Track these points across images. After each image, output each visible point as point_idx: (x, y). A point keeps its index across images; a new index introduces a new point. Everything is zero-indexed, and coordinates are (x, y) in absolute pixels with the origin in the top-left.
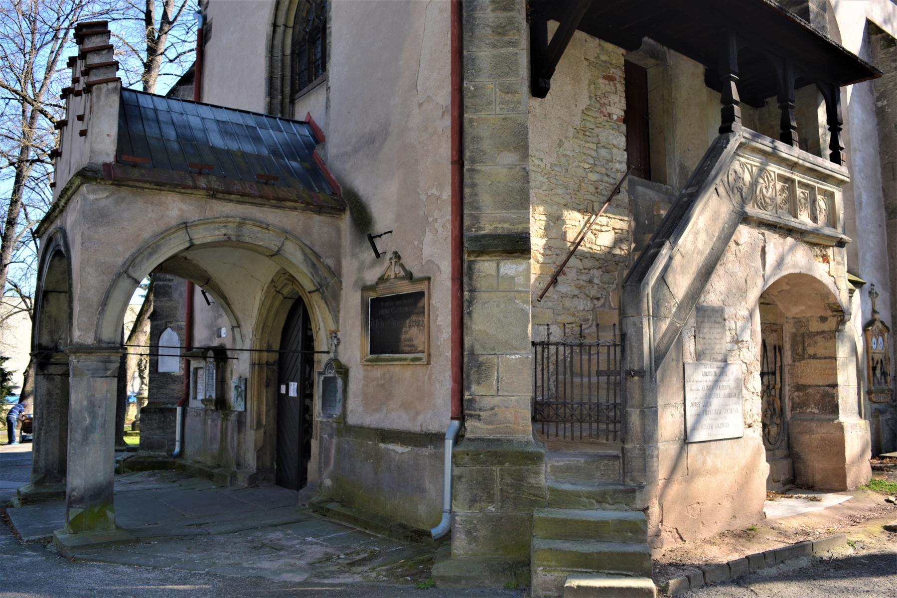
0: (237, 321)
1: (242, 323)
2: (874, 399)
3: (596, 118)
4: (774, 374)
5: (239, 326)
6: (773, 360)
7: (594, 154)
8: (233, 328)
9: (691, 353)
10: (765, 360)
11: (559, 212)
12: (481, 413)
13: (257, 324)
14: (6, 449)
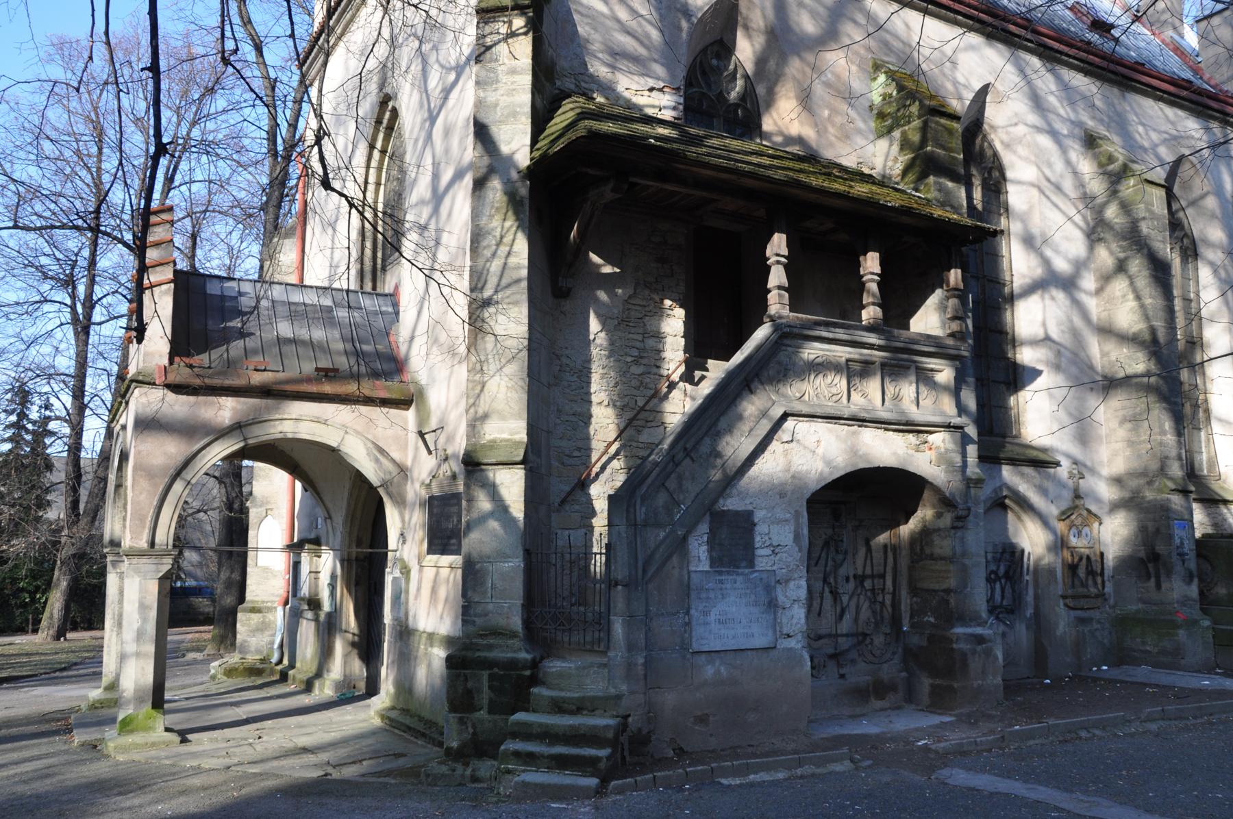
0: (328, 512)
1: (333, 515)
2: (1071, 605)
3: (645, 306)
4: (883, 576)
5: (330, 518)
6: (882, 561)
7: (638, 344)
8: (326, 518)
9: (51, 617)
10: (868, 562)
11: (945, 288)
12: (476, 619)
13: (347, 515)
14: (188, 720)
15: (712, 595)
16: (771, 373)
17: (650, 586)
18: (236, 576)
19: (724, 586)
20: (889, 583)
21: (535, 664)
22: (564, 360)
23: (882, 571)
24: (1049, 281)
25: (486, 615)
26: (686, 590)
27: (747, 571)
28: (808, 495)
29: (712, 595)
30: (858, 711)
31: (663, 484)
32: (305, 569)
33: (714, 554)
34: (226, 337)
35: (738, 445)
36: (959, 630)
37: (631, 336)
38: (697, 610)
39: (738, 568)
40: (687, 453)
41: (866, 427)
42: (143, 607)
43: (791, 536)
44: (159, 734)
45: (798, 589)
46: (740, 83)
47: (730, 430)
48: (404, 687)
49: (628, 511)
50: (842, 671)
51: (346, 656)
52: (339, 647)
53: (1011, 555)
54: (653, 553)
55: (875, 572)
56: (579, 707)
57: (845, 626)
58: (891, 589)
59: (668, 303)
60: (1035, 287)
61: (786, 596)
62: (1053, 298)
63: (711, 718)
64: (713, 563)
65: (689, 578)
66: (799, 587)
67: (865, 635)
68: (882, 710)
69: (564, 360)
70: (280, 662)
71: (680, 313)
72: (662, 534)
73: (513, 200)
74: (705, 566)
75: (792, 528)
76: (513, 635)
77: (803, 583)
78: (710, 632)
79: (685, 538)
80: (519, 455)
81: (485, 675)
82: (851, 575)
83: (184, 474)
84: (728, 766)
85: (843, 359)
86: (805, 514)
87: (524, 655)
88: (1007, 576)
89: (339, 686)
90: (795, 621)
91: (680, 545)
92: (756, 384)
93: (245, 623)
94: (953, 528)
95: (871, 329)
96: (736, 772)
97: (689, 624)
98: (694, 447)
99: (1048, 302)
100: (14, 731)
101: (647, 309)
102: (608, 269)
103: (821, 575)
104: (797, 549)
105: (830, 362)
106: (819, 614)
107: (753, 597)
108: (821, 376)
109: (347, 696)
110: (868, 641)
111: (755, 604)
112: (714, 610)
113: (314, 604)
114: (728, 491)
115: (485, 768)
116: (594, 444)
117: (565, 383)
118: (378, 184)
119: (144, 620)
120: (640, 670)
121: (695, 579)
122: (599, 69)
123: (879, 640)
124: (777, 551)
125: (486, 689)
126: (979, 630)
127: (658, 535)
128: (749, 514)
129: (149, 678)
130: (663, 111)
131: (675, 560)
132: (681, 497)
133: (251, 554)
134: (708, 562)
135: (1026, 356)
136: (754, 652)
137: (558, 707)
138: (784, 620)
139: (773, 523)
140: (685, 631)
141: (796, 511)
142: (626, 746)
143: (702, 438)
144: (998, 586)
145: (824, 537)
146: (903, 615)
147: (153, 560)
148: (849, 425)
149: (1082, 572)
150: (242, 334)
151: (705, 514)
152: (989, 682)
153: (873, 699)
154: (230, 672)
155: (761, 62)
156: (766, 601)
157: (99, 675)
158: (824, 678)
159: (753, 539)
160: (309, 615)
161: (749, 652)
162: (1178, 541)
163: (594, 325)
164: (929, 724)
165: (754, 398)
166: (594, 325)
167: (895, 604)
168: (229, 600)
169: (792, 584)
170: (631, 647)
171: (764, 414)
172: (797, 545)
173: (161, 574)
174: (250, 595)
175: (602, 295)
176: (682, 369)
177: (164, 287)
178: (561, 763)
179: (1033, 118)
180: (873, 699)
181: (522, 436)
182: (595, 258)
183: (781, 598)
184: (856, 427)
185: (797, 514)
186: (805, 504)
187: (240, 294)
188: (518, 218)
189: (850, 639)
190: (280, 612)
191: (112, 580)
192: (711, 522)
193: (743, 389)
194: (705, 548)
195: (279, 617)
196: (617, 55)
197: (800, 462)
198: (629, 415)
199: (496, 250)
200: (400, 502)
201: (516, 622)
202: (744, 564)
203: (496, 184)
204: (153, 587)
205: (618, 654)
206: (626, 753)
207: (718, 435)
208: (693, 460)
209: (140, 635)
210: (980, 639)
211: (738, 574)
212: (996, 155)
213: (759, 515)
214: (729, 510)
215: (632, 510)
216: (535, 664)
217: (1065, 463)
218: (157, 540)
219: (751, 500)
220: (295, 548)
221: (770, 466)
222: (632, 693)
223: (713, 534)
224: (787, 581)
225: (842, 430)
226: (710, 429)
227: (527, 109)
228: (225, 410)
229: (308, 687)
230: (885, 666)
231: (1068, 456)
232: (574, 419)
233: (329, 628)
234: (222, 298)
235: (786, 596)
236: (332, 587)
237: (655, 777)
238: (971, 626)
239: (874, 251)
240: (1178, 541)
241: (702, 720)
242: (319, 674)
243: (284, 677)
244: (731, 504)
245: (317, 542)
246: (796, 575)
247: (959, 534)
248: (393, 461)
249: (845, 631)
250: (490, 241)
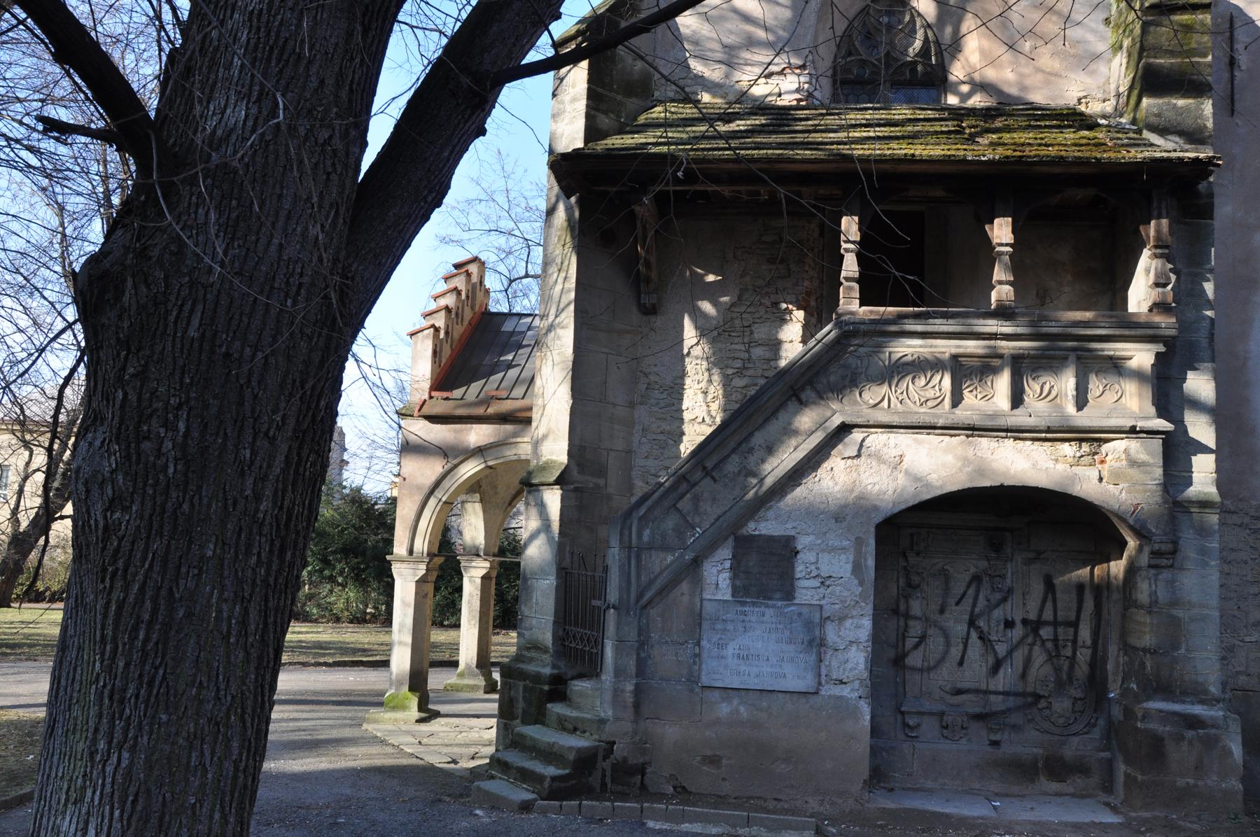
4: (1075, 625)
15: (730, 627)
16: (832, 378)
17: (653, 612)
19: (747, 619)
20: (1085, 634)
22: (652, 378)
23: (1073, 617)
25: (531, 629)
26: (697, 620)
27: (780, 603)
28: (879, 518)
29: (730, 627)
30: (1015, 789)
31: (674, 505)
33: (738, 583)
37: (733, 346)
38: (709, 641)
39: (770, 599)
40: (707, 473)
41: (982, 436)
43: (849, 567)
45: (861, 627)
46: (920, 34)
49: (622, 534)
50: (994, 737)
54: (656, 578)
55: (1059, 619)
57: (1006, 678)
58: (1089, 642)
61: (839, 636)
63: (724, 761)
64: (735, 591)
65: (701, 606)
66: (858, 627)
67: (1038, 697)
68: (1058, 794)
69: (652, 378)
72: (670, 558)
74: (725, 593)
75: (851, 558)
77: (867, 623)
78: (726, 667)
79: (696, 563)
81: (521, 684)
82: (1018, 620)
83: (436, 493)
84: (660, 809)
85: (947, 355)
86: (872, 542)
90: (849, 666)
92: (808, 394)
94: (1150, 566)
95: (1003, 313)
96: (667, 817)
97: (698, 655)
98: (716, 466)
100: (352, 698)
101: (756, 315)
102: (711, 278)
103: (967, 617)
104: (856, 582)
105: (927, 360)
106: (961, 663)
107: (787, 633)
108: (909, 378)
110: (1043, 704)
111: (790, 642)
112: (731, 643)
114: (761, 513)
117: (653, 401)
120: (629, 698)
121: (709, 608)
123: (1061, 705)
124: (828, 583)
125: (521, 699)
126: (1198, 710)
127: (665, 559)
130: (783, 97)
131: (685, 586)
132: (697, 520)
134: (730, 590)
136: (788, 695)
138: (834, 663)
139: (823, 551)
140: (694, 663)
141: (858, 539)
142: (608, 773)
143: (728, 456)
145: (973, 570)
146: (1110, 678)
147: (411, 565)
148: (952, 436)
151: (726, 539)
152: (1210, 783)
153: (1042, 778)
156: (807, 638)
158: (964, 741)
159: (793, 568)
161: (780, 694)
163: (690, 332)
164: (1064, 819)
166: (690, 332)
167: (1096, 664)
169: (848, 623)
170: (619, 672)
172: (857, 578)
173: (417, 578)
175: (707, 307)
177: (426, 332)
180: (1042, 778)
184: (963, 438)
185: (859, 542)
186: (873, 530)
189: (1011, 698)
192: (735, 548)
193: (789, 399)
194: (726, 575)
197: (870, 481)
202: (778, 595)
205: (607, 677)
206: (608, 780)
208: (715, 480)
210: (1193, 722)
211: (767, 606)
213: (802, 542)
214: (760, 536)
215: (626, 532)
218: (415, 549)
219: (795, 524)
222: (617, 719)
224: (842, 619)
225: (956, 442)
226: (740, 444)
228: (477, 435)
230: (1075, 740)
232: (661, 437)
235: (839, 636)
237: (561, 806)
238: (1184, 702)
239: (1004, 216)
241: (714, 761)
244: (766, 526)
246: (854, 613)
247: (1166, 575)
249: (1000, 688)
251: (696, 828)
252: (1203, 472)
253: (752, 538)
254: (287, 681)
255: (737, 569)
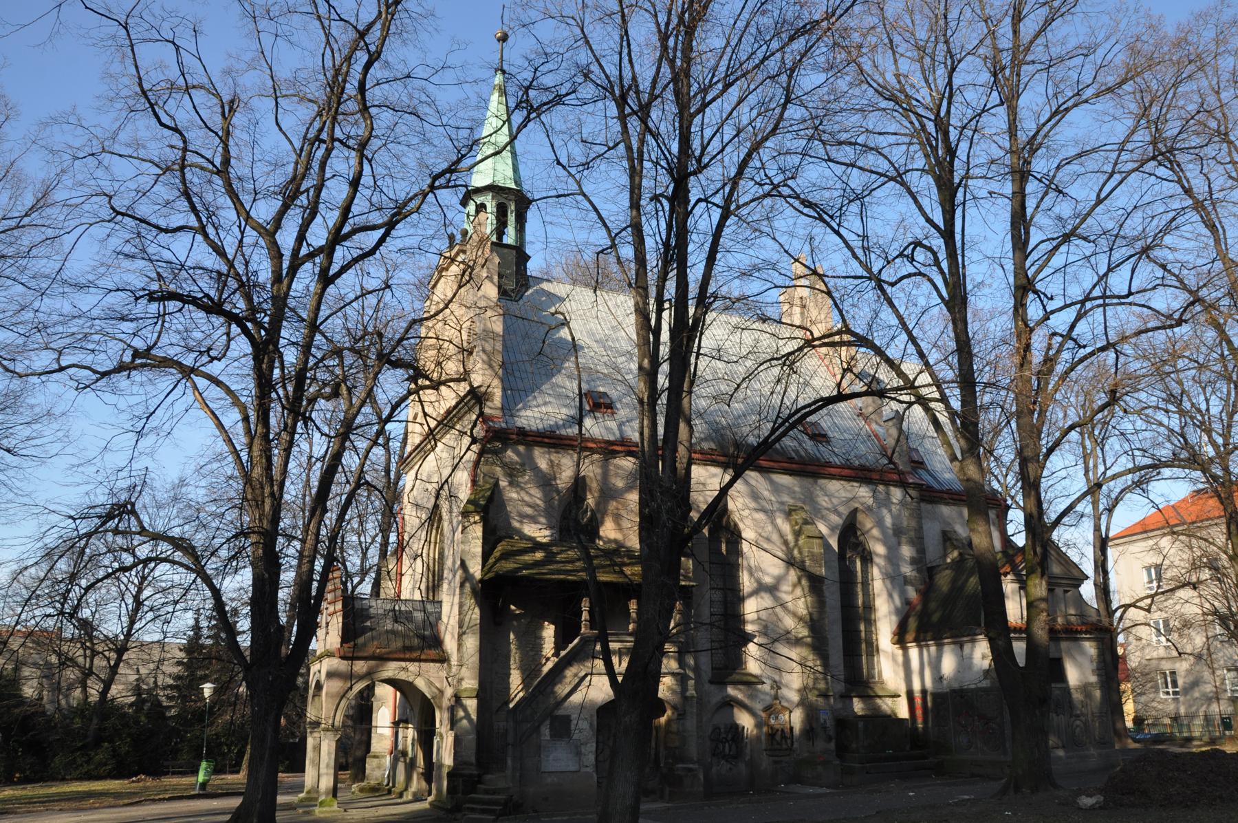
18: (365, 738)
21: (479, 776)
24: (761, 588)
32: (400, 736)
34: (365, 630)
35: (562, 689)
36: (680, 766)
42: (329, 753)
44: (335, 807)
45: (592, 747)
47: (560, 682)
48: (439, 790)
51: (418, 779)
52: (415, 777)
53: (737, 730)
56: (494, 792)
59: (546, 623)
60: (755, 593)
62: (762, 598)
64: (551, 737)
70: (388, 784)
71: (552, 627)
73: (474, 593)
76: (472, 764)
79: (539, 726)
80: (475, 694)
87: (475, 772)
88: (733, 739)
89: (415, 794)
91: (537, 729)
93: (370, 764)
99: (759, 600)
109: (417, 798)
113: (404, 754)
115: (459, 816)
116: (511, 686)
118: (436, 543)
119: (330, 758)
122: (516, 524)
126: (691, 766)
128: (569, 716)
129: (331, 784)
133: (373, 730)
135: (750, 628)
137: (487, 792)
144: (727, 745)
149: (778, 737)
150: (371, 629)
154: (362, 790)
155: (598, 504)
157: (303, 786)
160: (402, 759)
162: (822, 721)
163: (512, 636)
165: (571, 668)
167: (657, 754)
168: (359, 753)
171: (576, 675)
174: (373, 749)
176: (553, 651)
178: (483, 811)
179: (753, 505)
181: (476, 686)
182: (513, 607)
183: (583, 751)
187: (370, 607)
188: (476, 599)
190: (388, 758)
191: (310, 742)
195: (387, 761)
196: (523, 517)
198: (527, 673)
199: (782, 114)
200: (440, 708)
201: (473, 759)
203: (467, 585)
204: (333, 744)
205: (509, 772)
207: (555, 684)
209: (328, 766)
210: (690, 770)
212: (736, 525)
216: (479, 776)
217: (768, 681)
220: (396, 724)
221: (577, 698)
223: (551, 724)
227: (480, 554)
229: (401, 795)
231: (769, 677)
233: (411, 766)
234: (362, 609)
236: (413, 745)
240: (822, 721)
242: (406, 789)
243: (389, 792)
244: (561, 712)
245: (406, 722)
248: (437, 688)
250: (466, 608)
251: (559, 818)
252: (691, 692)
253: (557, 717)
254: (281, 799)
255: (551, 729)
